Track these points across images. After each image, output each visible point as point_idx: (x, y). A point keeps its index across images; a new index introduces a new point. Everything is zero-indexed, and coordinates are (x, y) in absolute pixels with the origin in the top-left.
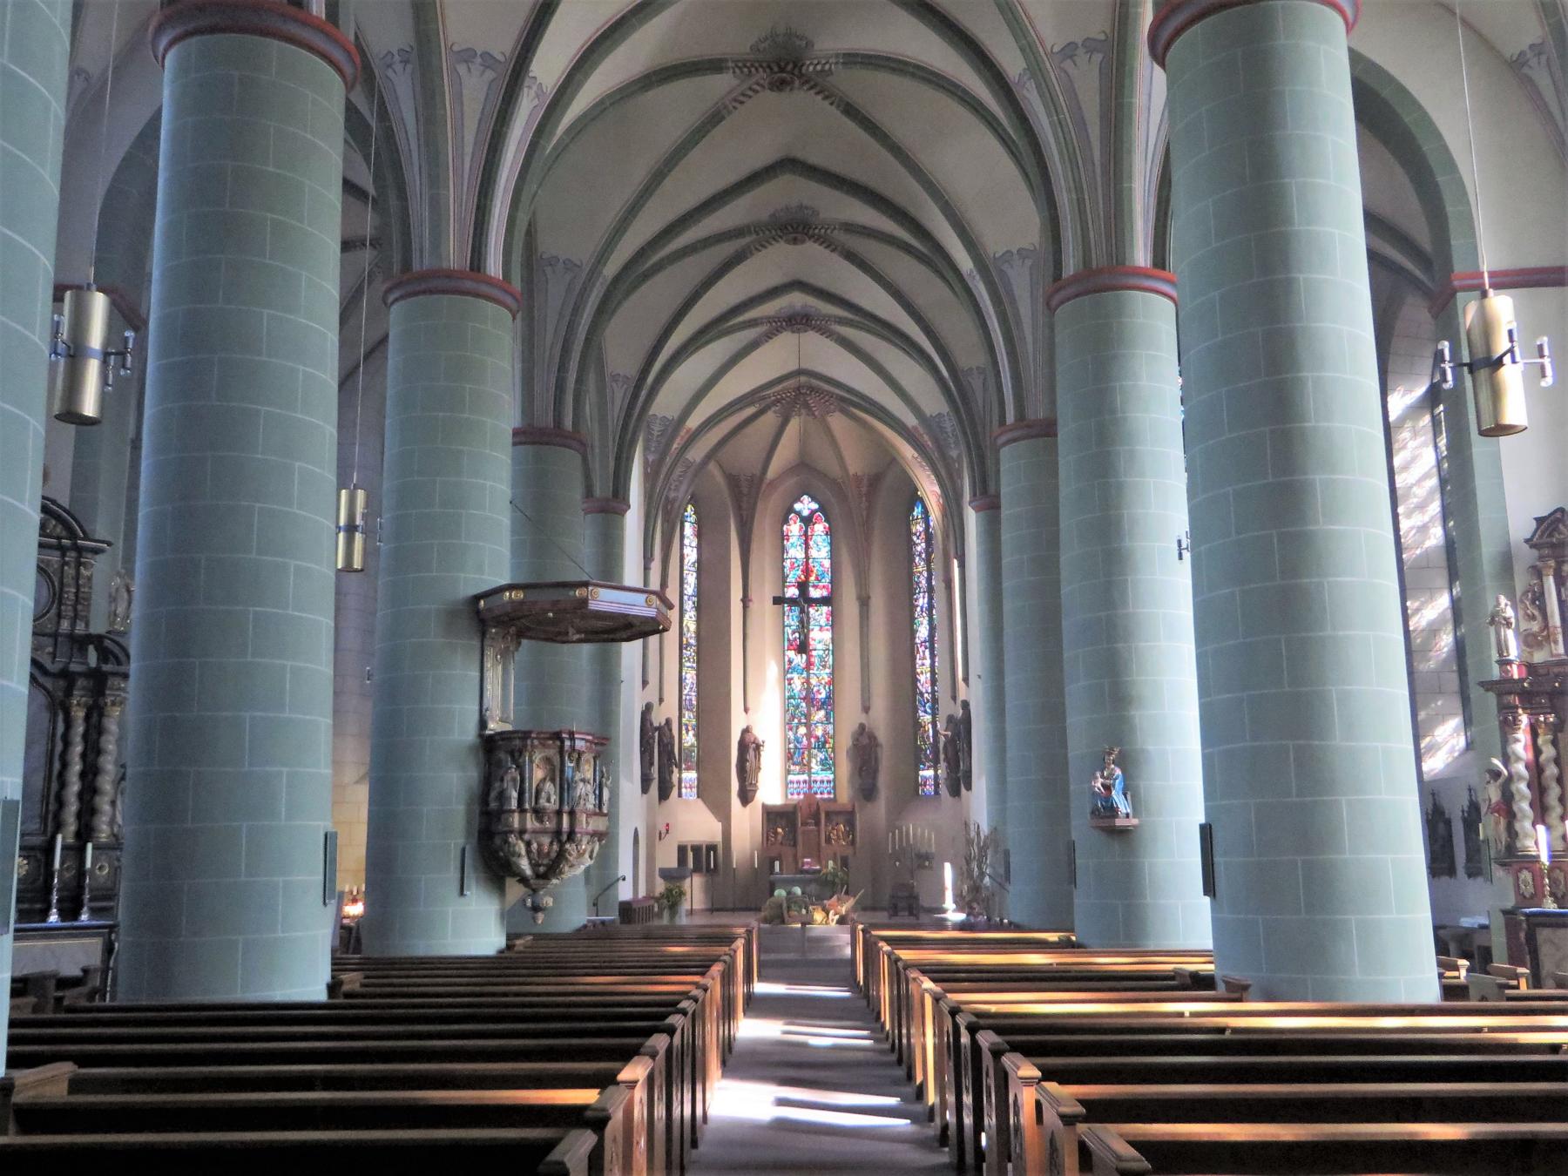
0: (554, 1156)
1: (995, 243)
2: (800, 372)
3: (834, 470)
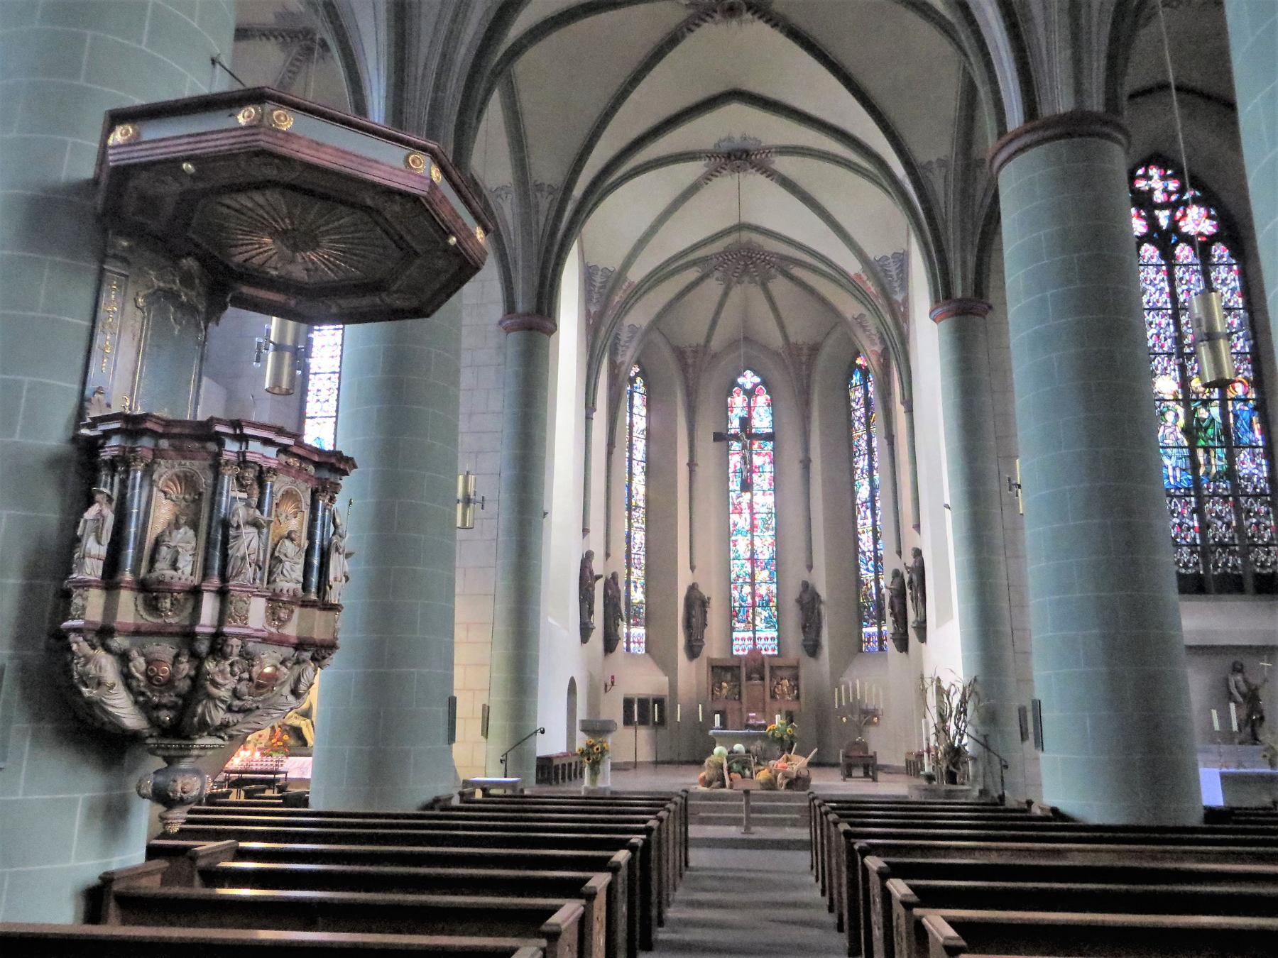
1: (922, 155)
2: (741, 227)
3: (776, 340)
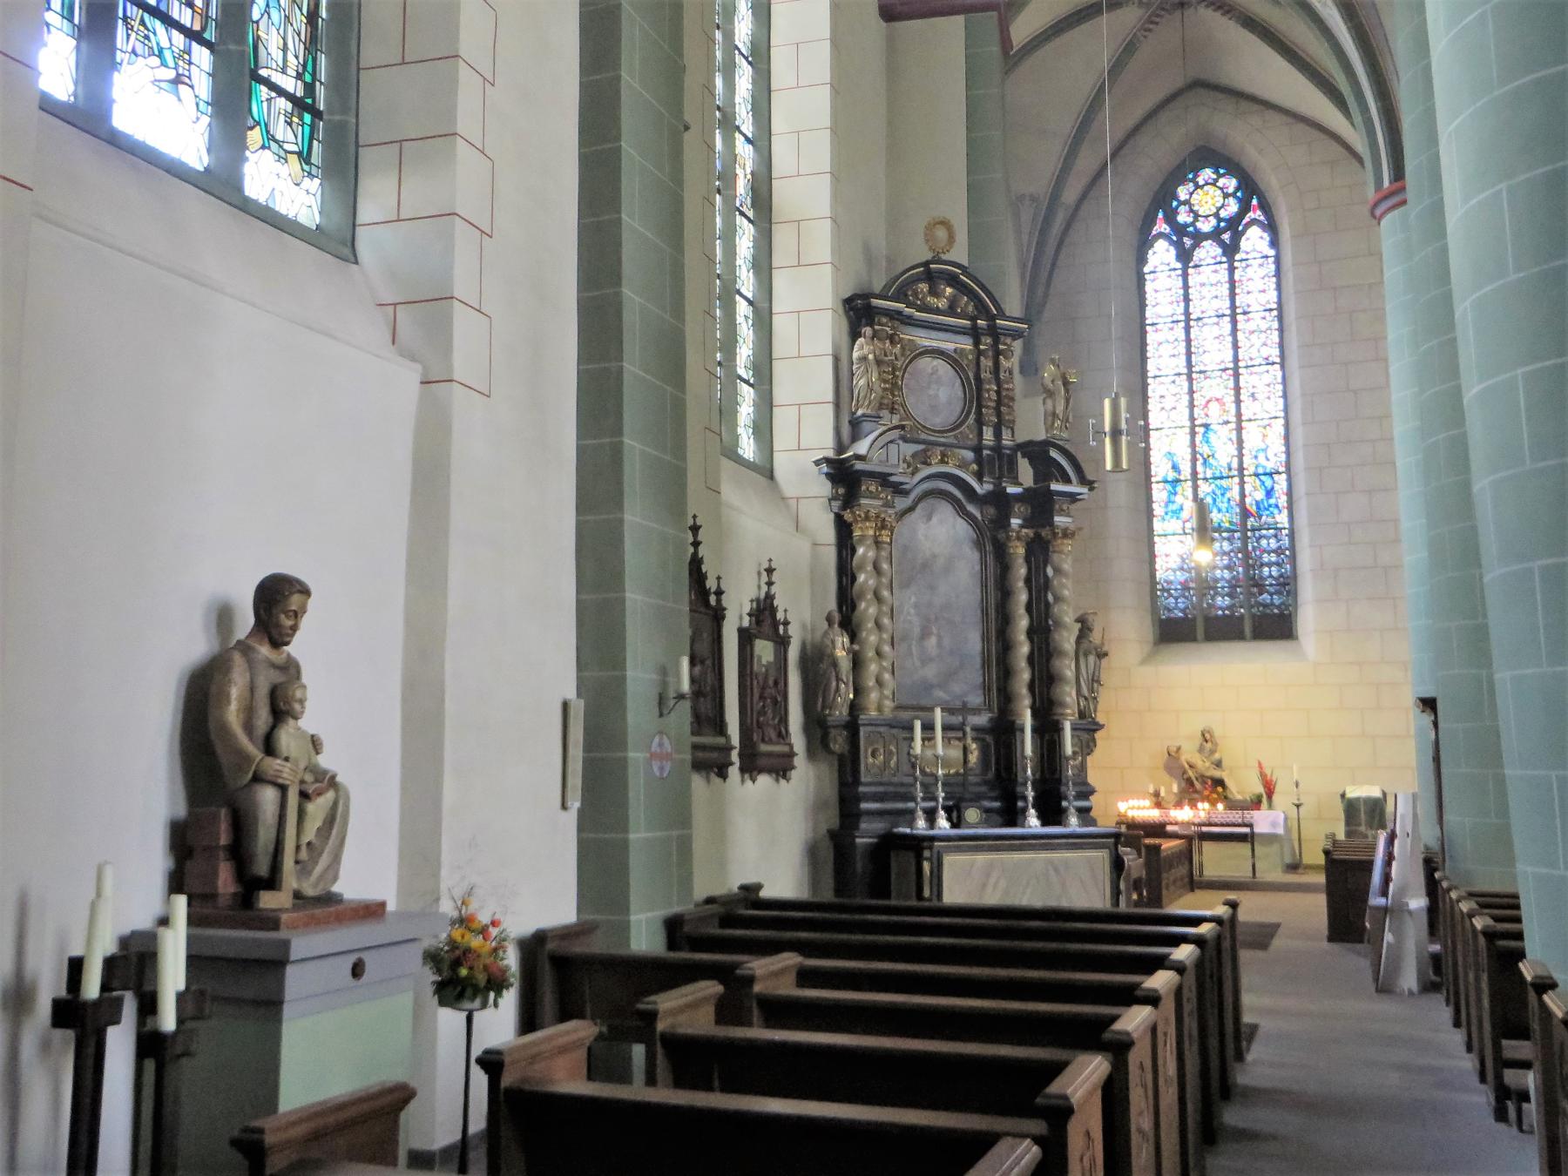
0: (1054, 1088)
